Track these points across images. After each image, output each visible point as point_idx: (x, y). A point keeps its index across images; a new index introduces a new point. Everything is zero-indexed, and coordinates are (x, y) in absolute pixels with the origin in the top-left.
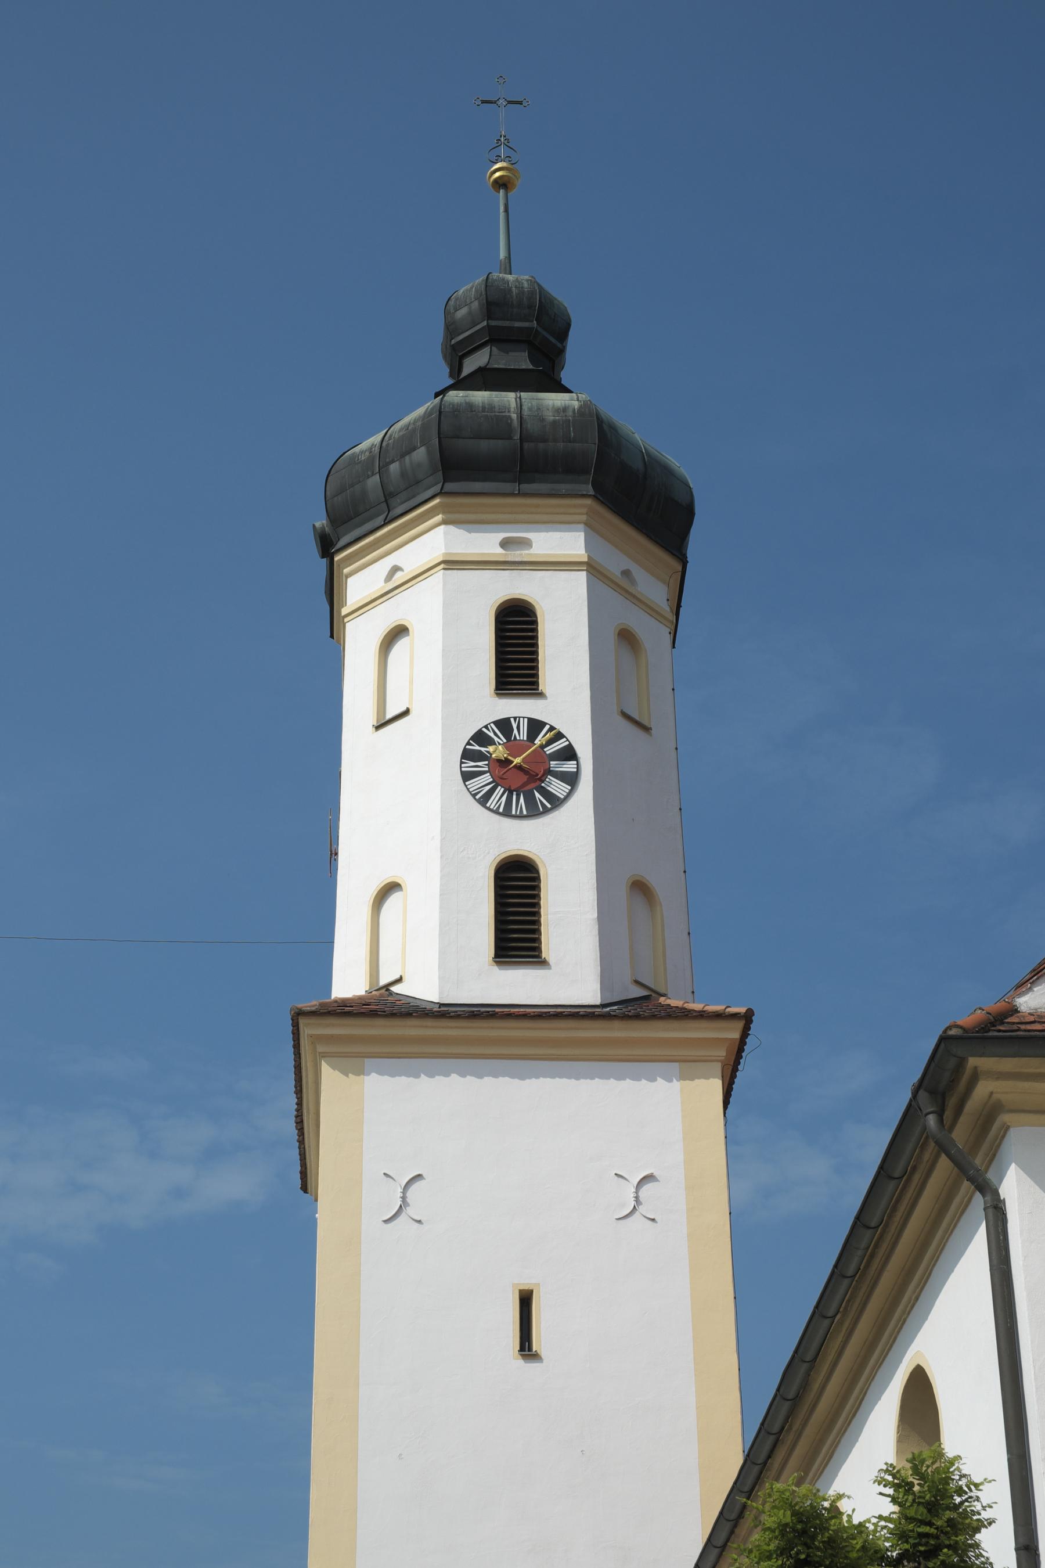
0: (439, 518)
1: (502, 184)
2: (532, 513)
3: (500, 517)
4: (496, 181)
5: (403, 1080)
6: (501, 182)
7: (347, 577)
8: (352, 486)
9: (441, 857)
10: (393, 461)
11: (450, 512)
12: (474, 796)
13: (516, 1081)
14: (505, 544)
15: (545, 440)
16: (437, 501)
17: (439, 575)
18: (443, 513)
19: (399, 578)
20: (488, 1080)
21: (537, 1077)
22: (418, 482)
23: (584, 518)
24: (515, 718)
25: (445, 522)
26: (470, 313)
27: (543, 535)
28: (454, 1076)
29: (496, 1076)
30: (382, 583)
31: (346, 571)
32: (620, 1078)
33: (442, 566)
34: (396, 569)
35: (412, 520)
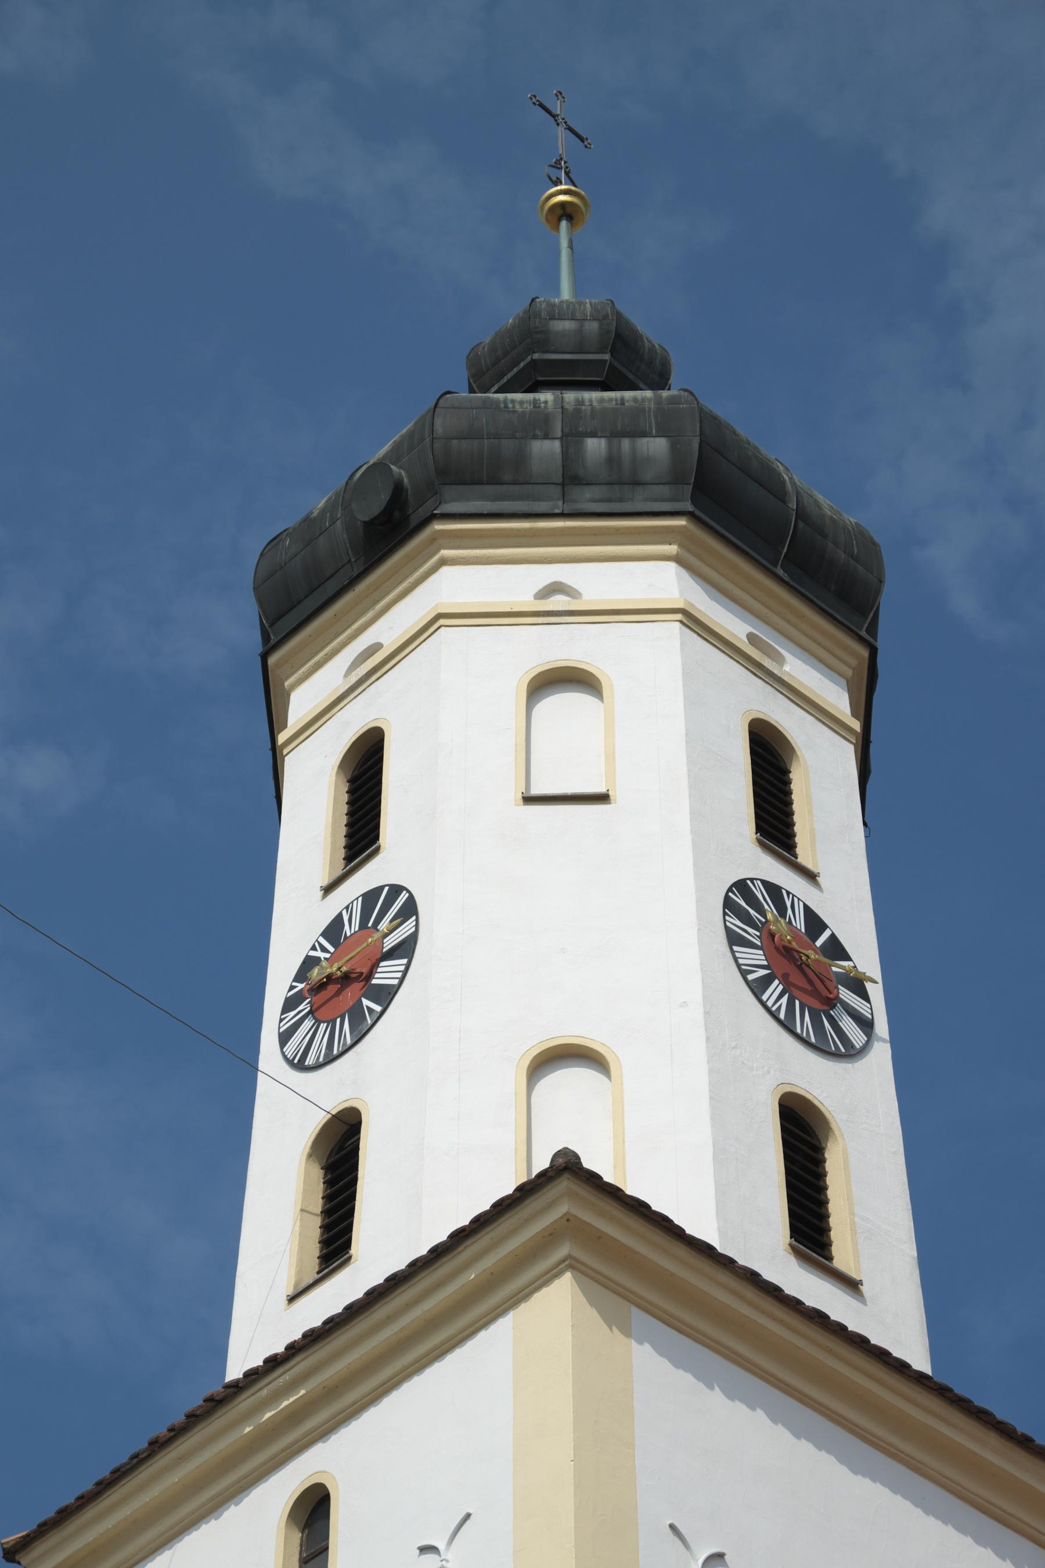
0: (673, 549)
1: (565, 212)
2: (788, 622)
3: (751, 602)
4: (562, 205)
5: (685, 1378)
6: (568, 210)
7: (444, 562)
8: (497, 436)
9: (708, 1039)
10: (593, 435)
11: (689, 550)
12: (744, 974)
13: (843, 1470)
14: (752, 638)
15: (824, 536)
16: (681, 522)
17: (672, 630)
18: (680, 545)
19: (559, 602)
20: (805, 1447)
21: (874, 1480)
22: (636, 483)
23: (849, 673)
24: (314, 948)
25: (677, 559)
26: (580, 331)
27: (798, 662)
28: (760, 1413)
29: (819, 1447)
30: (529, 597)
31: (446, 553)
32: (979, 1541)
33: (679, 616)
34: (555, 588)
35: (617, 530)
